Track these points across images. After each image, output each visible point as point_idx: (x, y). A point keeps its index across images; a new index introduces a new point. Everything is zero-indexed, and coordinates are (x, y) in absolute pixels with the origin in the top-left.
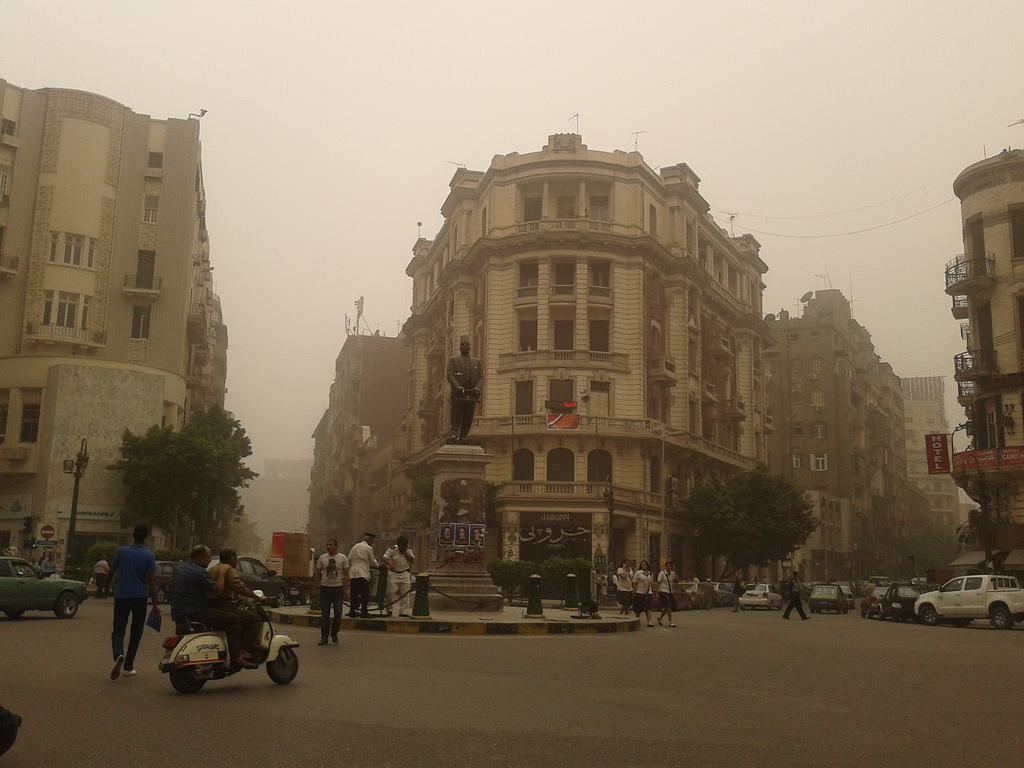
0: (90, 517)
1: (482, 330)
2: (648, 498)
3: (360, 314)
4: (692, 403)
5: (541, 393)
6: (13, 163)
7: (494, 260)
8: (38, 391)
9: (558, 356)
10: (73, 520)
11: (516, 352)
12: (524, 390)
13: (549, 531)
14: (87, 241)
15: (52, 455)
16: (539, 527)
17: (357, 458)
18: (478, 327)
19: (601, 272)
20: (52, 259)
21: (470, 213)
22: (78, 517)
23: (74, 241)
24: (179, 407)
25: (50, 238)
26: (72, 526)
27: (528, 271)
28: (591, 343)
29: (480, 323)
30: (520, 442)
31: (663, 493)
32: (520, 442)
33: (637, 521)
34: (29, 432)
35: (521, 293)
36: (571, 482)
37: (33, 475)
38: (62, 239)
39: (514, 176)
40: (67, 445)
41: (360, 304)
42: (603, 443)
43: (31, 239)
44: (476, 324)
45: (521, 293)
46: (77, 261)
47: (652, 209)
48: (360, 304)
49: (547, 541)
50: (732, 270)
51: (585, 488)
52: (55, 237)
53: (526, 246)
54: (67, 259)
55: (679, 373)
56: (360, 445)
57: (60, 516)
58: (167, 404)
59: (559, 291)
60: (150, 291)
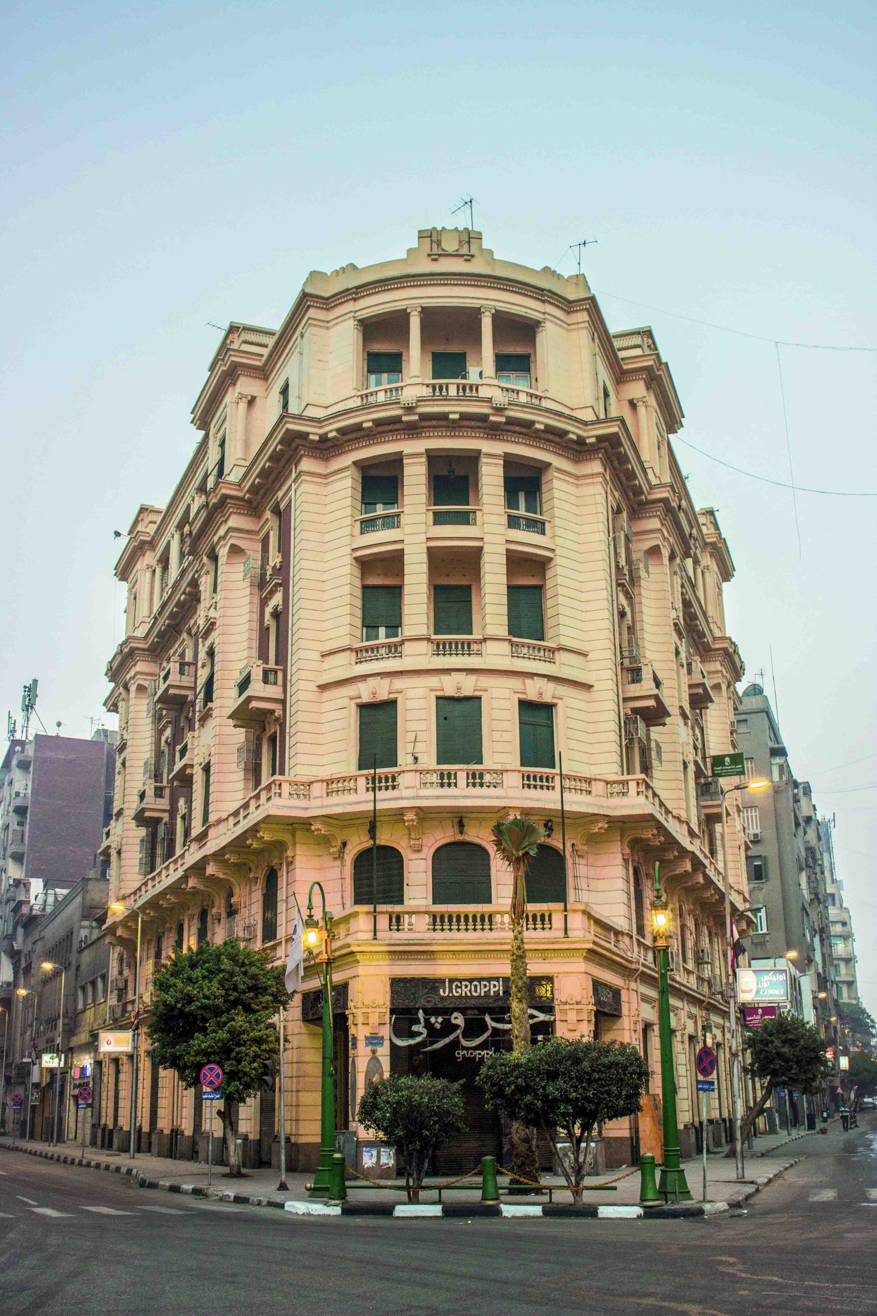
5: (417, 730)
7: (306, 464)
9: (441, 649)
11: (358, 645)
12: (377, 728)
13: (458, 1019)
16: (436, 1012)
17: (20, 931)
18: (163, 739)
19: (525, 482)
21: (252, 402)
27: (380, 484)
28: (510, 626)
29: (277, 599)
30: (372, 831)
32: (372, 831)
36: (398, 908)
39: (349, 307)
42: (461, 825)
44: (264, 602)
45: (367, 525)
48: (31, 692)
49: (456, 1044)
51: (427, 919)
56: (25, 910)
59: (439, 519)
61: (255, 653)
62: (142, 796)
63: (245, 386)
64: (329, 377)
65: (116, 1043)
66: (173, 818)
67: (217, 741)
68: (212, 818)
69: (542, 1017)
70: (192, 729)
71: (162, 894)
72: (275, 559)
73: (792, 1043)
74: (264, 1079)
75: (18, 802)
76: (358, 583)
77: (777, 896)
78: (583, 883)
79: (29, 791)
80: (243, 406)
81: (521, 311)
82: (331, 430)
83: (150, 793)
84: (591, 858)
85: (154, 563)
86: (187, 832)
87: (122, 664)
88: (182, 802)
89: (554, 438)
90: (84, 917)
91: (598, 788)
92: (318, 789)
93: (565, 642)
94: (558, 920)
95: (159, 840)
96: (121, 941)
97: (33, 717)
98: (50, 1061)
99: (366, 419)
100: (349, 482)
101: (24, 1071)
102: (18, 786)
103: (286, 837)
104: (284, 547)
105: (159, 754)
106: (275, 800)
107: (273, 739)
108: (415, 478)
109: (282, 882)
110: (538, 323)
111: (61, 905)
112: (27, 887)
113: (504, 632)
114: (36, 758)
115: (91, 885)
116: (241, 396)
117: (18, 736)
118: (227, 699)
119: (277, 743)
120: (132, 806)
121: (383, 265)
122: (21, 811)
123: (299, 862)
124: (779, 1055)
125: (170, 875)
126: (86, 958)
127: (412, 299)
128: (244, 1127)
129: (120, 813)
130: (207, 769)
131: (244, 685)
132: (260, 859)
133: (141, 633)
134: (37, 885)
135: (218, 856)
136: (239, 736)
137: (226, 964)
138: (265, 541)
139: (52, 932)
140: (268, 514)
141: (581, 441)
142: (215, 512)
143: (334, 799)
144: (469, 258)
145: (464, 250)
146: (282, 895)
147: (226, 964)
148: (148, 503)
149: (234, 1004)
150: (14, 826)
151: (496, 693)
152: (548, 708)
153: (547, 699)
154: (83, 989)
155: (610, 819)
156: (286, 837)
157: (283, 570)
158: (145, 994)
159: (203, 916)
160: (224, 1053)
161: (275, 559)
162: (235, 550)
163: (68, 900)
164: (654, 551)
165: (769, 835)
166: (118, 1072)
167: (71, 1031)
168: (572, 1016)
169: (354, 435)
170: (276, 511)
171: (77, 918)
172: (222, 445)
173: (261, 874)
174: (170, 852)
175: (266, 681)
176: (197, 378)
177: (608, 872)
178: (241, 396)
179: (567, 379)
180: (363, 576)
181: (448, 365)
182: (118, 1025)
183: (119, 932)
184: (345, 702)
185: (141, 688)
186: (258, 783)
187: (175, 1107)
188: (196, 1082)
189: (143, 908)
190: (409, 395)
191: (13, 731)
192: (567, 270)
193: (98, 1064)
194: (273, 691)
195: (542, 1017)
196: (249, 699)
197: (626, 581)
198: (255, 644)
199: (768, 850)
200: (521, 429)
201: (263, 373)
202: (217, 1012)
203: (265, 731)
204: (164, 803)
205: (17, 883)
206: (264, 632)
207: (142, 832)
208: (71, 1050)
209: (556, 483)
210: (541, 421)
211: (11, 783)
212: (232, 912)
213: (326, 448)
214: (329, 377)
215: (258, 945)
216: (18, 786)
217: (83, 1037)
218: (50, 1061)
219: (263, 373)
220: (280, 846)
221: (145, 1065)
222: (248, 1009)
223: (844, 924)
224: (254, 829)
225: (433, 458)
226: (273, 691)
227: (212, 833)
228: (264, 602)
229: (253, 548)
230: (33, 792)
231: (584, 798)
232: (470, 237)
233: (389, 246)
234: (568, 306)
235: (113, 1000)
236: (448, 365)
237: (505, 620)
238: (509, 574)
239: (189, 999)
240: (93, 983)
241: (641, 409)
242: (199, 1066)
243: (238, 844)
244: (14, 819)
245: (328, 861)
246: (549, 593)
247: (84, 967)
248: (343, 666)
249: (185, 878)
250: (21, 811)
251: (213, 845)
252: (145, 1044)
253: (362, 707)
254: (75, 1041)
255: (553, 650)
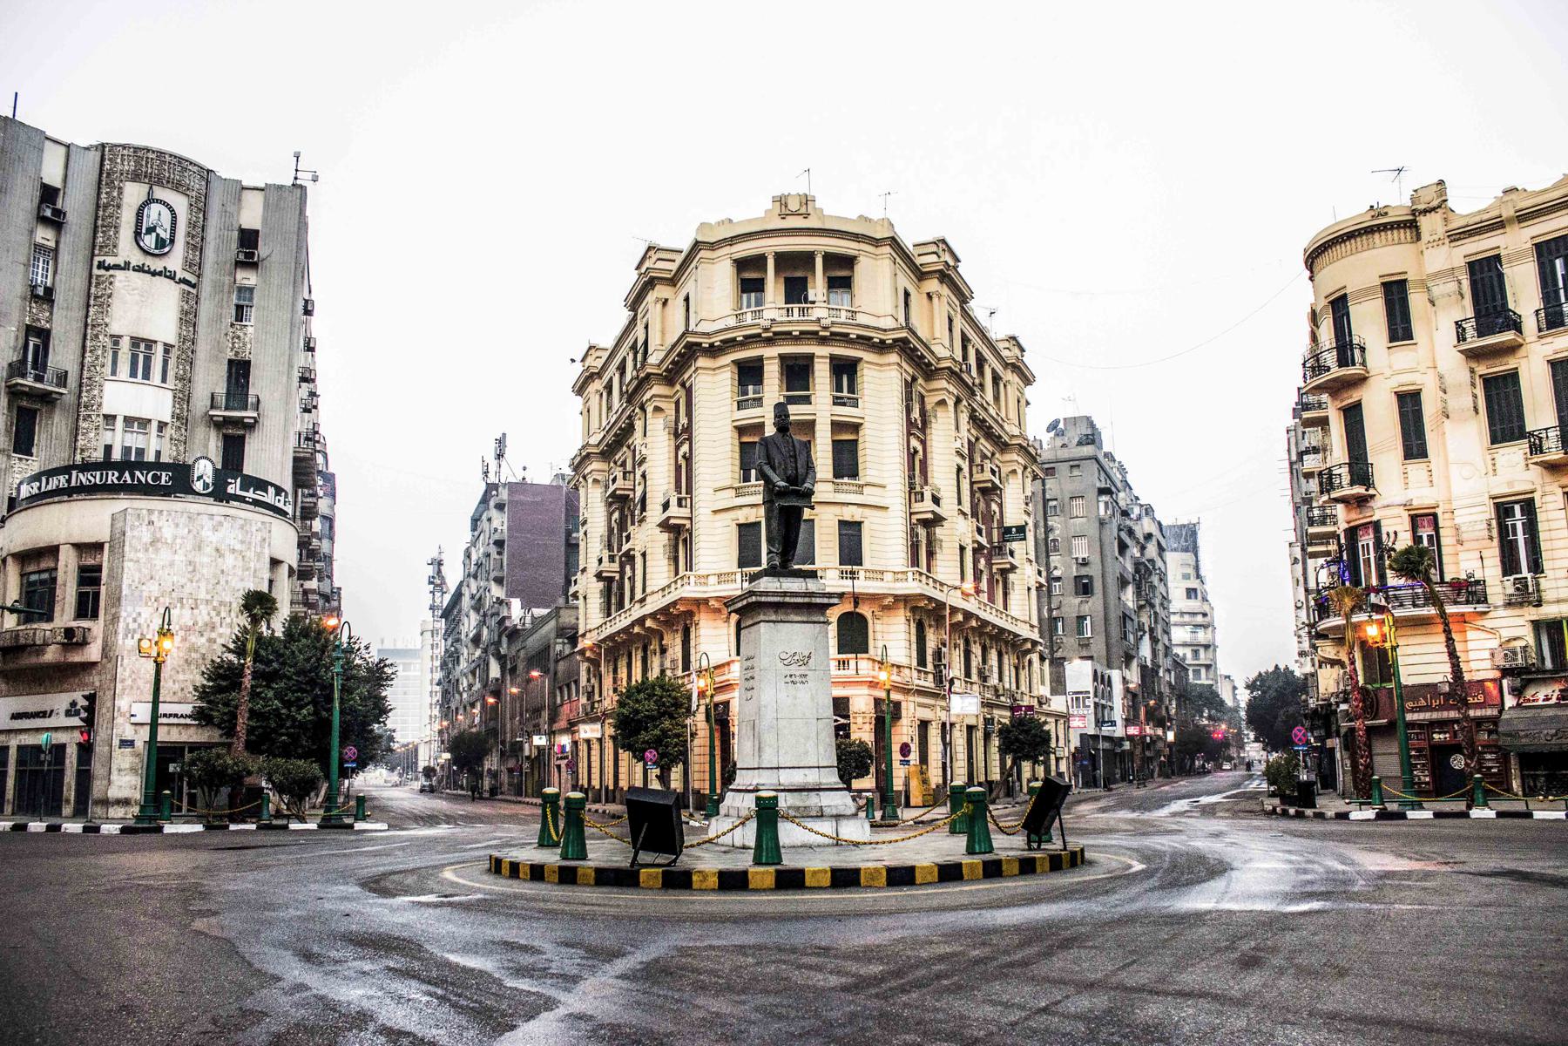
0: (175, 721)
1: (688, 459)
2: (915, 674)
3: (500, 456)
4: (962, 549)
6: (57, 243)
7: (702, 362)
8: (99, 547)
10: (154, 725)
14: (159, 349)
15: (120, 637)
17: (504, 640)
18: (681, 453)
19: (845, 370)
20: (114, 373)
21: (665, 302)
22: (161, 721)
23: (142, 346)
24: (290, 567)
25: (109, 345)
26: (153, 733)
27: (750, 373)
29: (685, 448)
31: (930, 667)
33: (904, 705)
34: (87, 606)
35: (741, 405)
37: (94, 664)
38: (125, 344)
39: (727, 250)
40: (141, 620)
41: (501, 442)
43: (84, 347)
44: (677, 448)
45: (741, 405)
46: (146, 376)
47: (907, 294)
48: (501, 442)
50: (996, 379)
52: (116, 343)
53: (751, 340)
54: (133, 374)
55: (948, 508)
56: (508, 623)
57: (133, 720)
58: (275, 563)
60: (243, 414)
61: (673, 486)
62: (600, 561)
63: (661, 291)
64: (714, 300)
65: (589, 731)
66: (622, 577)
67: (648, 538)
68: (648, 590)
69: (842, 721)
70: (633, 523)
71: (619, 632)
72: (684, 420)
73: (1027, 732)
74: (683, 756)
75: (497, 537)
76: (737, 443)
77: (1100, 608)
78: (879, 636)
79: (505, 527)
80: (659, 305)
81: (842, 251)
82: (716, 340)
83: (606, 559)
84: (885, 619)
85: (601, 388)
86: (632, 598)
87: (580, 463)
88: (628, 568)
89: (865, 342)
90: (558, 636)
91: (888, 577)
92: (713, 580)
93: (869, 480)
94: (852, 663)
95: (614, 593)
96: (588, 660)
97: (503, 463)
98: (540, 741)
99: (739, 335)
100: (729, 375)
101: (517, 749)
102: (496, 523)
103: (694, 608)
104: (689, 414)
105: (611, 530)
106: (687, 587)
107: (685, 540)
108: (772, 371)
109: (692, 636)
110: (855, 258)
111: (539, 623)
112: (508, 605)
113: (830, 476)
114: (510, 502)
115: (562, 612)
116: (658, 300)
117: (492, 479)
118: (654, 514)
119: (688, 543)
120: (593, 567)
121: (749, 221)
122: (499, 544)
123: (702, 623)
124: (1017, 740)
125: (622, 622)
126: (562, 666)
127: (769, 246)
128: (673, 785)
129: (584, 570)
130: (644, 555)
131: (666, 506)
132: (679, 618)
133: (594, 440)
134: (516, 603)
135: (653, 615)
136: (664, 537)
137: (658, 691)
138: (677, 403)
139: (533, 642)
140: (678, 387)
141: (883, 342)
142: (643, 382)
143: (723, 586)
144: (806, 216)
145: (803, 210)
146: (692, 643)
147: (658, 691)
148: (593, 342)
149: (663, 714)
150: (494, 555)
151: (824, 517)
152: (857, 525)
153: (858, 519)
154: (561, 689)
155: (895, 596)
156: (694, 608)
157: (688, 429)
158: (609, 701)
159: (645, 649)
160: (657, 743)
161: (684, 420)
162: (657, 409)
163: (544, 620)
164: (942, 403)
165: (1095, 559)
166: (589, 749)
167: (553, 719)
168: (860, 720)
169: (730, 344)
170: (683, 385)
171: (553, 635)
172: (646, 327)
173: (680, 628)
174: (621, 605)
175: (680, 505)
176: (629, 279)
177: (893, 628)
178: (658, 300)
179: (877, 297)
180: (740, 436)
181: (796, 291)
182: (591, 718)
183: (588, 654)
184: (729, 522)
185: (596, 481)
186: (677, 573)
187: (630, 773)
188: (641, 758)
189: (604, 641)
190: (769, 314)
191: (486, 473)
192: (876, 215)
193: (575, 743)
194: (685, 512)
195: (842, 721)
196: (669, 518)
197: (918, 427)
198: (673, 480)
199: (1094, 571)
200: (844, 338)
201: (673, 281)
202: (653, 718)
203: (679, 535)
204: (616, 566)
205: (500, 602)
206: (678, 468)
207: (601, 585)
208: (554, 733)
209: (865, 372)
210: (854, 333)
211: (489, 520)
212: (663, 651)
213: (714, 351)
214: (714, 300)
215: (680, 673)
216: (496, 523)
217: (562, 724)
218: (540, 741)
219: (673, 281)
220: (690, 614)
221: (609, 745)
222: (672, 717)
223: (1205, 615)
224: (674, 604)
225: (783, 358)
226: (685, 512)
227: (649, 599)
228: (677, 448)
229: (669, 407)
230: (509, 528)
231: (879, 584)
232: (806, 200)
233: (752, 209)
234: (876, 242)
235: (583, 700)
236: (796, 291)
237: (831, 468)
238: (833, 432)
239: (637, 712)
240: (568, 686)
241: (935, 300)
242: (644, 750)
243: (664, 610)
244: (493, 550)
245: (720, 623)
246: (860, 446)
247: (560, 675)
248: (728, 499)
249: (632, 625)
250: (499, 544)
251: (650, 608)
252: (610, 731)
253: (740, 525)
254: (556, 727)
255: (862, 486)
